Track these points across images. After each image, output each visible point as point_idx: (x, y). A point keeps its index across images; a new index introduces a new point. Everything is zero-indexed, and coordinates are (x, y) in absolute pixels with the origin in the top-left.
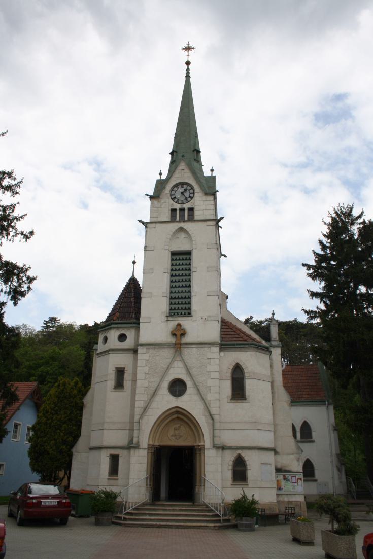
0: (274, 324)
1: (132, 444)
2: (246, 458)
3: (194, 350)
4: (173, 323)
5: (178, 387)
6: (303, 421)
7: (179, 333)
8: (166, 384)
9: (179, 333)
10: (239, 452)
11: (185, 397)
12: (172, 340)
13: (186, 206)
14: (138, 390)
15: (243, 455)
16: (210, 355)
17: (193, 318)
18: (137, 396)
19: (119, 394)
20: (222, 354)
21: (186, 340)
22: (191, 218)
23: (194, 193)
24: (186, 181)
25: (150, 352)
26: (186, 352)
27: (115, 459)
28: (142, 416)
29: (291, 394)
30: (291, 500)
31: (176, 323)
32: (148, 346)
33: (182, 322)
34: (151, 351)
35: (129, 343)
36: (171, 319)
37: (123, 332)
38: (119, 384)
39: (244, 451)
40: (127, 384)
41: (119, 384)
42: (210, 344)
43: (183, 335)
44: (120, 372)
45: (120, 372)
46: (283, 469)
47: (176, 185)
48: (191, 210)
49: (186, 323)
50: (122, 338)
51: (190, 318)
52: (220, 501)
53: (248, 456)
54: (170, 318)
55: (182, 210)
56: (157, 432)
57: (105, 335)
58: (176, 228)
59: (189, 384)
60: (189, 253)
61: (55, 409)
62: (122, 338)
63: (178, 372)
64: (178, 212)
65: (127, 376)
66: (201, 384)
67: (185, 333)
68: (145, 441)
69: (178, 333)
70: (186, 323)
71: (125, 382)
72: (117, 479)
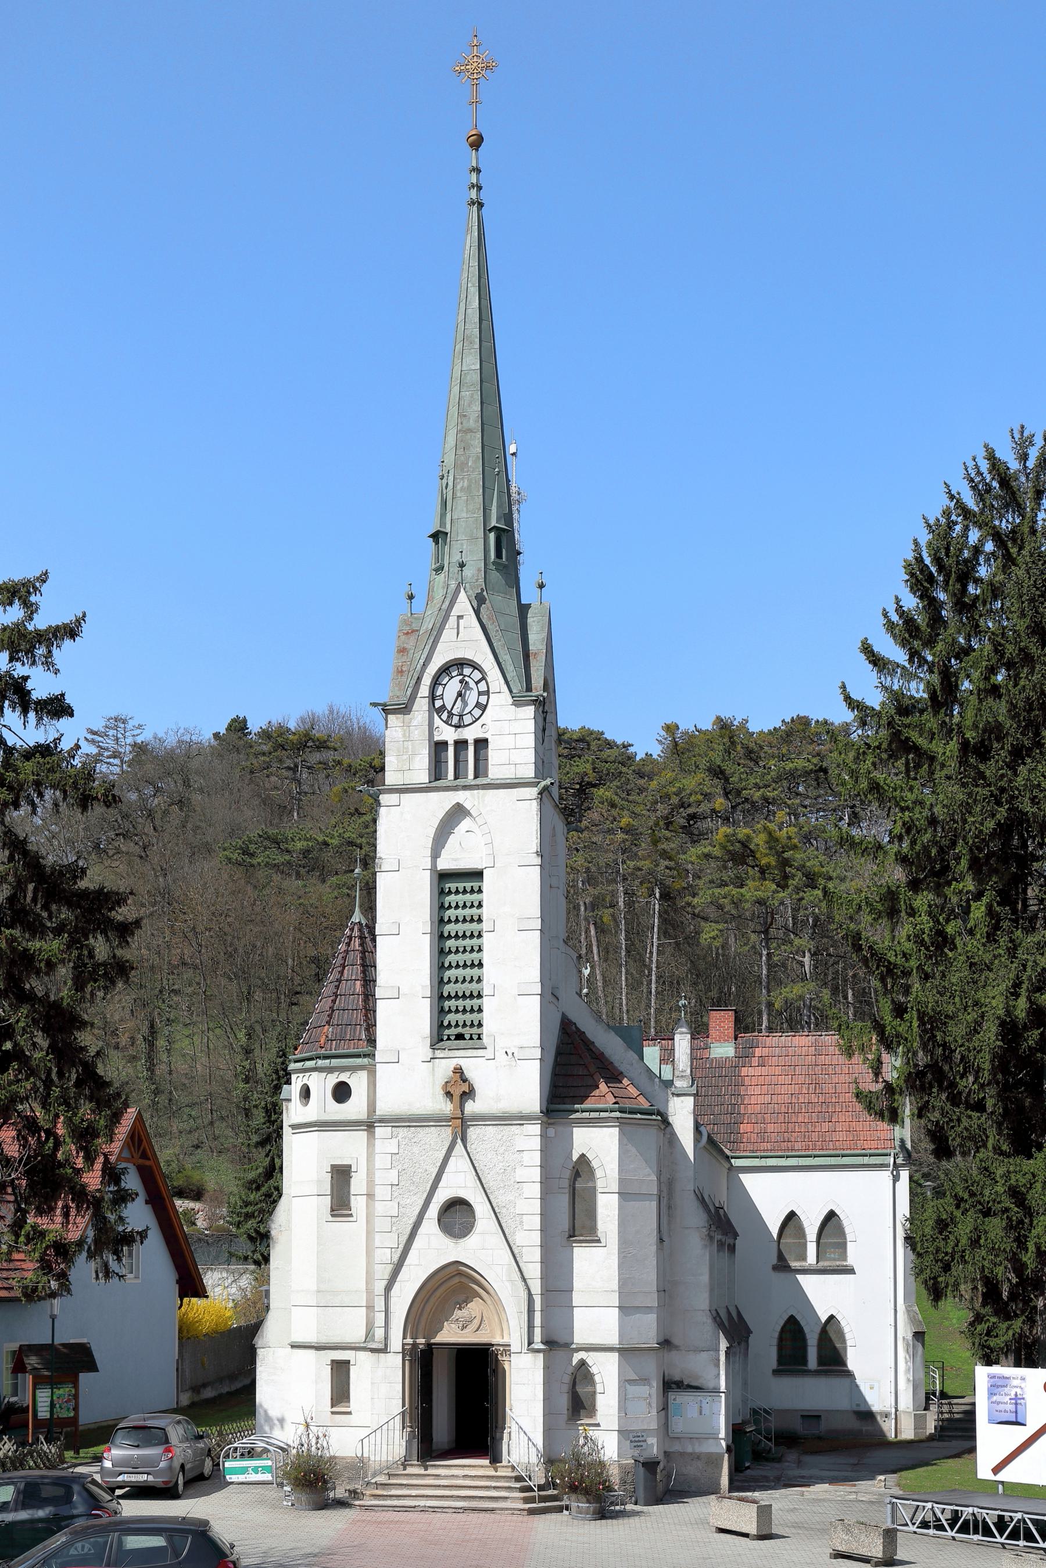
0: (967, 808)
1: (373, 1341)
2: (594, 1370)
3: (490, 1132)
4: (445, 1067)
5: (456, 1215)
9: (460, 1089)
11: (472, 1241)
12: (447, 1107)
13: (470, 734)
14: (378, 1164)
15: (589, 1362)
16: (521, 1143)
17: (488, 1053)
18: (377, 1237)
19: (341, 1227)
20: (551, 1132)
21: (470, 1107)
23: (487, 693)
24: (469, 655)
25: (400, 1136)
27: (341, 1371)
28: (388, 1288)
29: (913, 1185)
31: (452, 1063)
32: (397, 1121)
33: (464, 1063)
34: (402, 1132)
35: (355, 1107)
36: (442, 1055)
37: (344, 1077)
38: (340, 1204)
39: (591, 1353)
40: (358, 1204)
41: (340, 1204)
42: (522, 1118)
43: (469, 1094)
44: (341, 1175)
45: (341, 1175)
47: (445, 670)
48: (481, 744)
49: (475, 1066)
50: (342, 1093)
51: (480, 1052)
56: (803, 1477)
57: (305, 1081)
58: (448, 806)
59: (481, 1208)
60: (478, 875)
62: (342, 1093)
63: (459, 1182)
65: (358, 1184)
69: (457, 1092)
70: (476, 1066)
71: (352, 1198)
72: (350, 1413)
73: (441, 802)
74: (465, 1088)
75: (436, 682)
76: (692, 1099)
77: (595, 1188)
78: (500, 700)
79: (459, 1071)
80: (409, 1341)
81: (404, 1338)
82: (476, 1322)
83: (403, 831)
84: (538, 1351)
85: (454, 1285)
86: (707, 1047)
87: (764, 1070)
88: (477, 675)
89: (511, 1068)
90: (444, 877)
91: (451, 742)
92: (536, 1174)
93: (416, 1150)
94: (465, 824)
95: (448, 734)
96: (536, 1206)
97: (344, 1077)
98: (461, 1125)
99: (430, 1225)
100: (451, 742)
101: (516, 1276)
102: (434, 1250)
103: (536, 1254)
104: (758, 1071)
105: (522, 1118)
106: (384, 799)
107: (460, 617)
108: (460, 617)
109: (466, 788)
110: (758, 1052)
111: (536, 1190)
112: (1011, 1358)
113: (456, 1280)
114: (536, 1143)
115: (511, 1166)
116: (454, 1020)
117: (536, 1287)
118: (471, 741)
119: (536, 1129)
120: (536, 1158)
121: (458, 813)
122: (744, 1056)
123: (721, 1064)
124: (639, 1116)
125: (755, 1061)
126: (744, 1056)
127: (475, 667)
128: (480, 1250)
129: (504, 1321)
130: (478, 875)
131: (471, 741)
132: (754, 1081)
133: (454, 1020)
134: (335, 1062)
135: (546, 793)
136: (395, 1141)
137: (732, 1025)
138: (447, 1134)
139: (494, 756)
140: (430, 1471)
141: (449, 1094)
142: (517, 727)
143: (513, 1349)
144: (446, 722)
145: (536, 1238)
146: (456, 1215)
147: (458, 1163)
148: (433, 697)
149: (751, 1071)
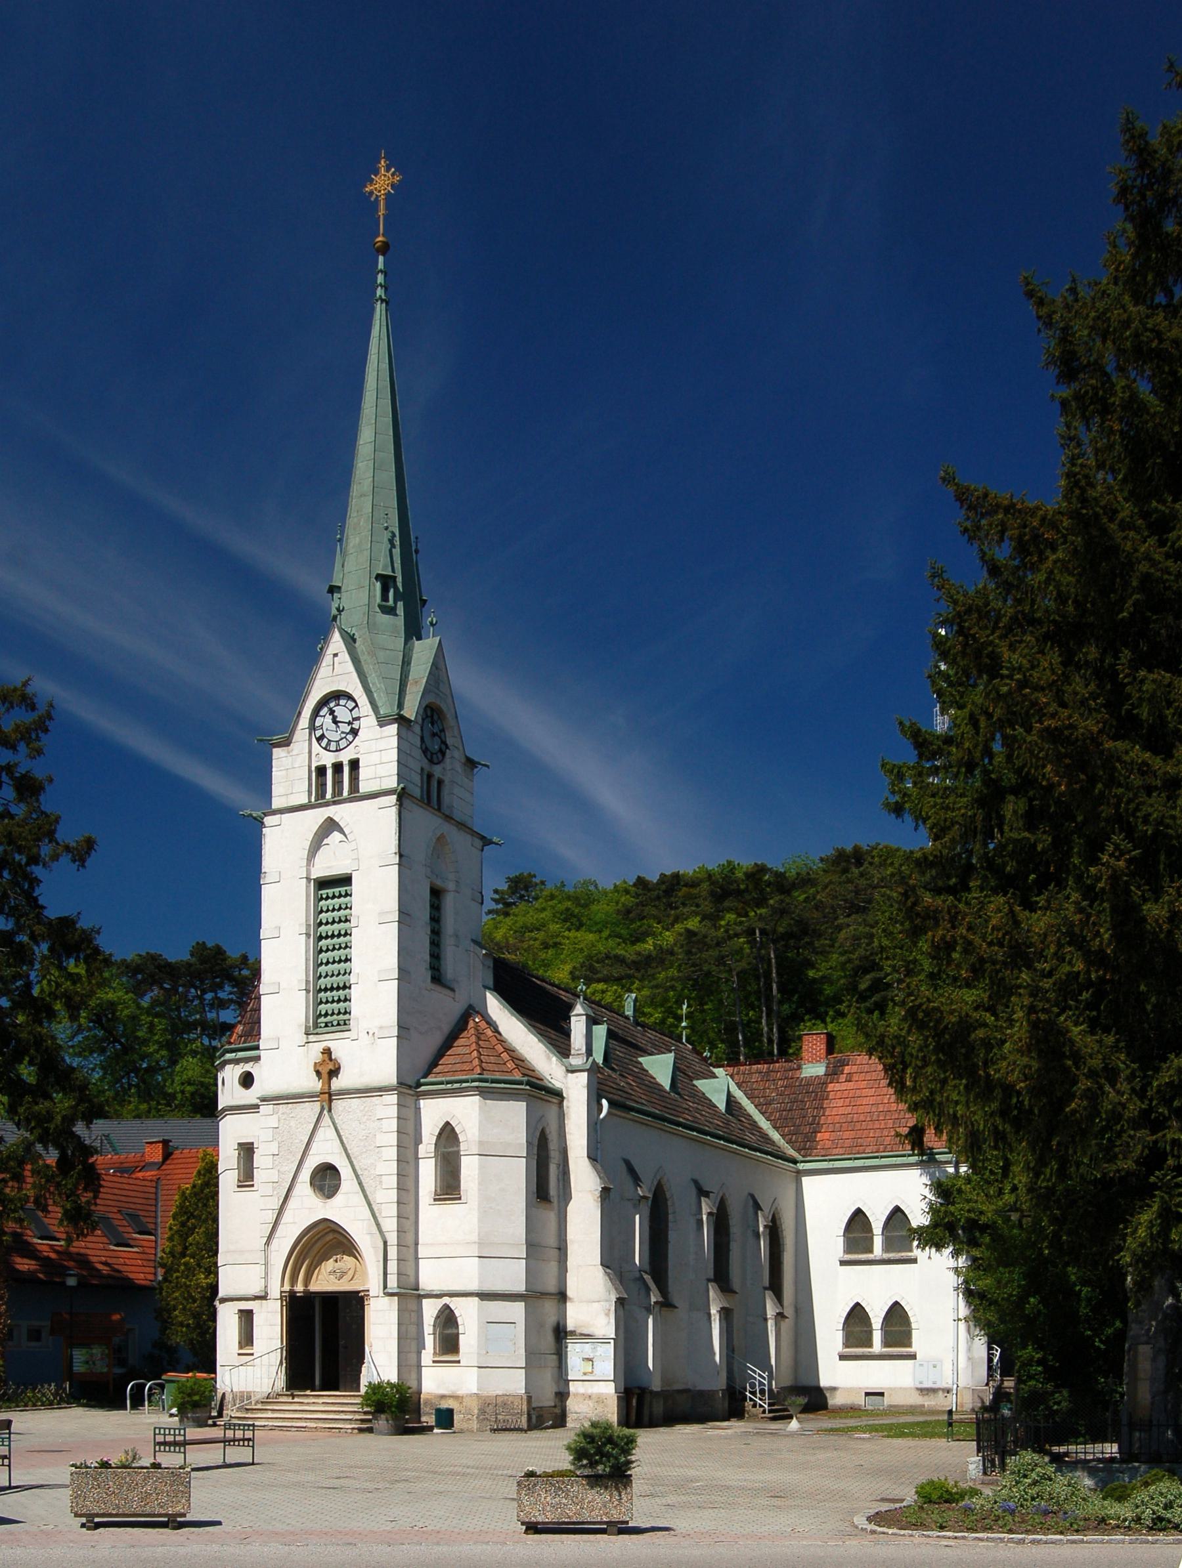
3: (354, 1103)
5: (326, 1179)
6: (891, 1208)
7: (329, 1068)
8: (305, 1175)
9: (329, 1068)
10: (446, 1300)
11: (339, 1198)
12: (317, 1085)
13: (345, 757)
19: (246, 1195)
21: (336, 1084)
22: (356, 795)
24: (342, 687)
26: (339, 1105)
30: (590, 1391)
33: (332, 1045)
42: (382, 1090)
43: (334, 1072)
46: (578, 1331)
47: (324, 702)
48: (355, 764)
49: (341, 1047)
51: (346, 1034)
52: (633, 1458)
53: (456, 1304)
54: (312, 1038)
55: (338, 767)
59: (345, 1172)
60: (346, 880)
61: (189, 1224)
63: (325, 1150)
64: (329, 772)
66: (366, 1173)
67: (339, 1068)
68: (275, 1291)
69: (324, 1071)
70: (341, 1047)
73: (317, 817)
74: (331, 1066)
75: (316, 713)
76: (585, 1074)
77: (458, 1152)
78: (368, 723)
79: (327, 1052)
80: (287, 1288)
81: (282, 1286)
82: (351, 1273)
83: (284, 849)
84: (392, 1295)
85: (326, 1241)
86: (799, 1068)
87: (851, 1085)
88: (351, 704)
89: (371, 1048)
90: (323, 883)
91: (329, 765)
92: (393, 1139)
93: (293, 1123)
94: (336, 835)
95: (328, 759)
96: (393, 1167)
97: (248, 1067)
98: (328, 1097)
99: (304, 1186)
100: (329, 765)
101: (375, 1229)
102: (307, 1208)
103: (393, 1210)
104: (844, 1086)
105: (382, 1090)
106: (268, 820)
107: (335, 655)
108: (335, 655)
109: (327, 804)
110: (847, 1069)
111: (393, 1153)
112: (124, 1140)
113: (330, 1236)
114: (393, 1111)
115: (368, 1132)
116: (329, 1007)
117: (392, 1239)
118: (346, 763)
119: (393, 1099)
120: (393, 1125)
121: (331, 826)
122: (833, 1073)
123: (810, 1081)
124: (503, 1085)
125: (843, 1078)
126: (833, 1073)
127: (350, 697)
128: (345, 1209)
129: (368, 1274)
130: (346, 880)
131: (346, 763)
132: (839, 1095)
133: (329, 1007)
134: (241, 1054)
135: (406, 802)
136: (275, 1116)
137: (823, 1046)
138: (317, 1107)
139: (363, 773)
140: (296, 1400)
141: (318, 1073)
142: (382, 744)
143: (371, 1293)
144: (325, 749)
145: (393, 1195)
146: (326, 1179)
147: (326, 1133)
148: (312, 727)
149: (837, 1087)
